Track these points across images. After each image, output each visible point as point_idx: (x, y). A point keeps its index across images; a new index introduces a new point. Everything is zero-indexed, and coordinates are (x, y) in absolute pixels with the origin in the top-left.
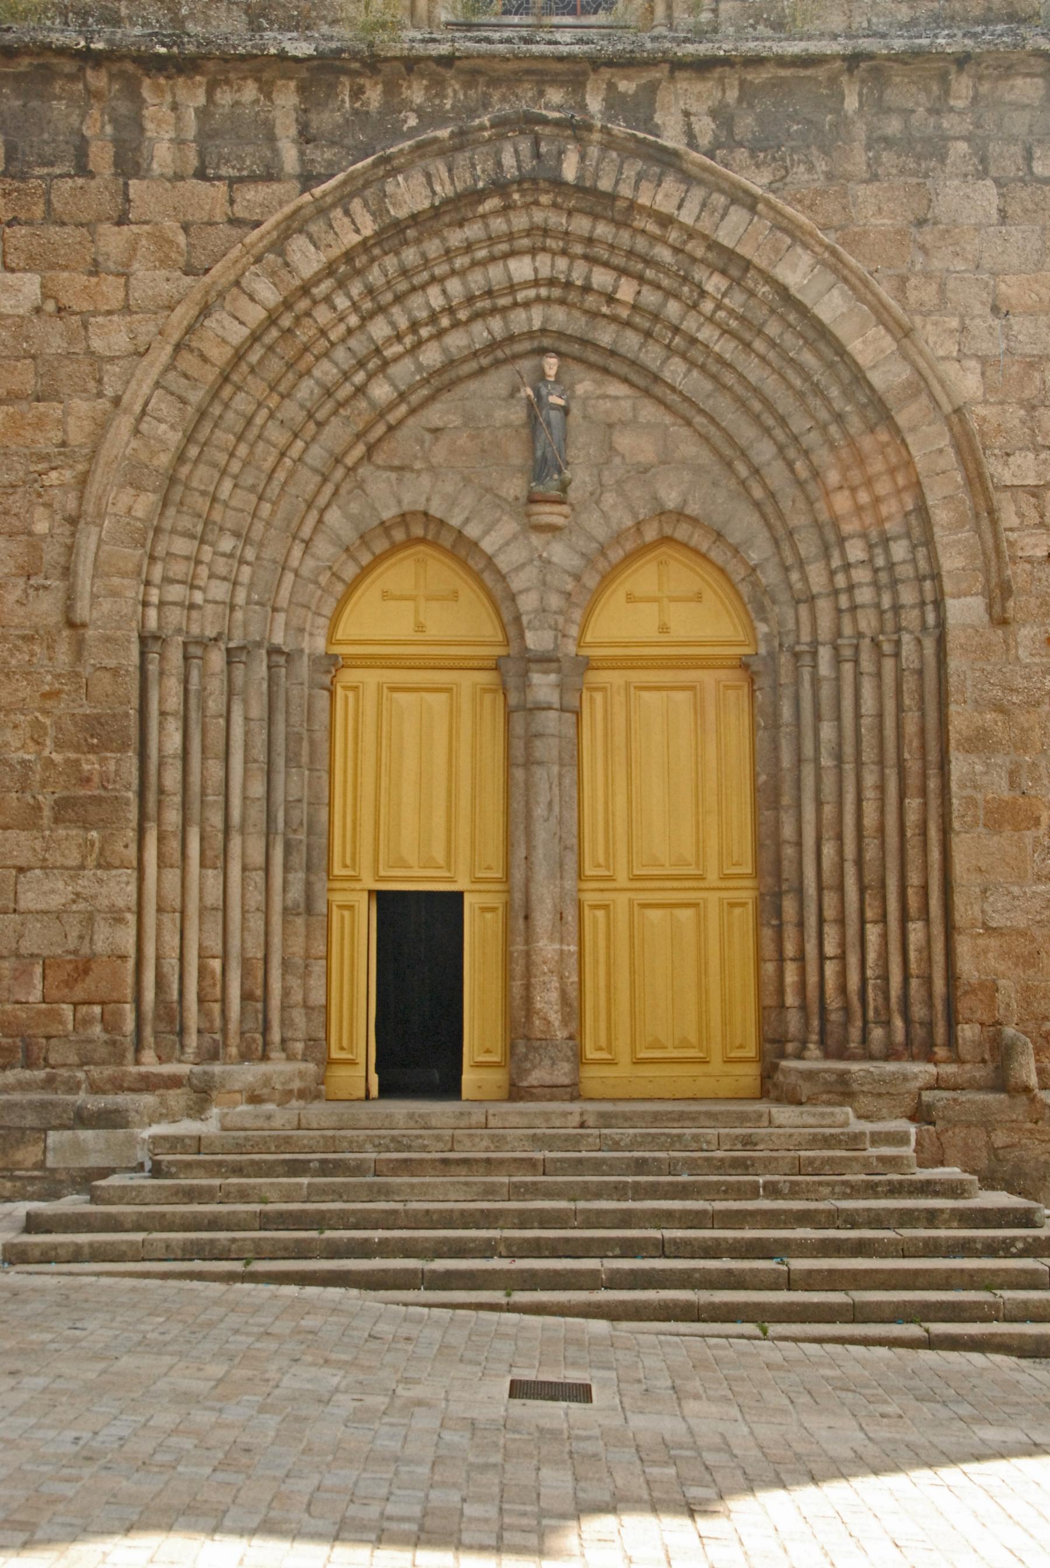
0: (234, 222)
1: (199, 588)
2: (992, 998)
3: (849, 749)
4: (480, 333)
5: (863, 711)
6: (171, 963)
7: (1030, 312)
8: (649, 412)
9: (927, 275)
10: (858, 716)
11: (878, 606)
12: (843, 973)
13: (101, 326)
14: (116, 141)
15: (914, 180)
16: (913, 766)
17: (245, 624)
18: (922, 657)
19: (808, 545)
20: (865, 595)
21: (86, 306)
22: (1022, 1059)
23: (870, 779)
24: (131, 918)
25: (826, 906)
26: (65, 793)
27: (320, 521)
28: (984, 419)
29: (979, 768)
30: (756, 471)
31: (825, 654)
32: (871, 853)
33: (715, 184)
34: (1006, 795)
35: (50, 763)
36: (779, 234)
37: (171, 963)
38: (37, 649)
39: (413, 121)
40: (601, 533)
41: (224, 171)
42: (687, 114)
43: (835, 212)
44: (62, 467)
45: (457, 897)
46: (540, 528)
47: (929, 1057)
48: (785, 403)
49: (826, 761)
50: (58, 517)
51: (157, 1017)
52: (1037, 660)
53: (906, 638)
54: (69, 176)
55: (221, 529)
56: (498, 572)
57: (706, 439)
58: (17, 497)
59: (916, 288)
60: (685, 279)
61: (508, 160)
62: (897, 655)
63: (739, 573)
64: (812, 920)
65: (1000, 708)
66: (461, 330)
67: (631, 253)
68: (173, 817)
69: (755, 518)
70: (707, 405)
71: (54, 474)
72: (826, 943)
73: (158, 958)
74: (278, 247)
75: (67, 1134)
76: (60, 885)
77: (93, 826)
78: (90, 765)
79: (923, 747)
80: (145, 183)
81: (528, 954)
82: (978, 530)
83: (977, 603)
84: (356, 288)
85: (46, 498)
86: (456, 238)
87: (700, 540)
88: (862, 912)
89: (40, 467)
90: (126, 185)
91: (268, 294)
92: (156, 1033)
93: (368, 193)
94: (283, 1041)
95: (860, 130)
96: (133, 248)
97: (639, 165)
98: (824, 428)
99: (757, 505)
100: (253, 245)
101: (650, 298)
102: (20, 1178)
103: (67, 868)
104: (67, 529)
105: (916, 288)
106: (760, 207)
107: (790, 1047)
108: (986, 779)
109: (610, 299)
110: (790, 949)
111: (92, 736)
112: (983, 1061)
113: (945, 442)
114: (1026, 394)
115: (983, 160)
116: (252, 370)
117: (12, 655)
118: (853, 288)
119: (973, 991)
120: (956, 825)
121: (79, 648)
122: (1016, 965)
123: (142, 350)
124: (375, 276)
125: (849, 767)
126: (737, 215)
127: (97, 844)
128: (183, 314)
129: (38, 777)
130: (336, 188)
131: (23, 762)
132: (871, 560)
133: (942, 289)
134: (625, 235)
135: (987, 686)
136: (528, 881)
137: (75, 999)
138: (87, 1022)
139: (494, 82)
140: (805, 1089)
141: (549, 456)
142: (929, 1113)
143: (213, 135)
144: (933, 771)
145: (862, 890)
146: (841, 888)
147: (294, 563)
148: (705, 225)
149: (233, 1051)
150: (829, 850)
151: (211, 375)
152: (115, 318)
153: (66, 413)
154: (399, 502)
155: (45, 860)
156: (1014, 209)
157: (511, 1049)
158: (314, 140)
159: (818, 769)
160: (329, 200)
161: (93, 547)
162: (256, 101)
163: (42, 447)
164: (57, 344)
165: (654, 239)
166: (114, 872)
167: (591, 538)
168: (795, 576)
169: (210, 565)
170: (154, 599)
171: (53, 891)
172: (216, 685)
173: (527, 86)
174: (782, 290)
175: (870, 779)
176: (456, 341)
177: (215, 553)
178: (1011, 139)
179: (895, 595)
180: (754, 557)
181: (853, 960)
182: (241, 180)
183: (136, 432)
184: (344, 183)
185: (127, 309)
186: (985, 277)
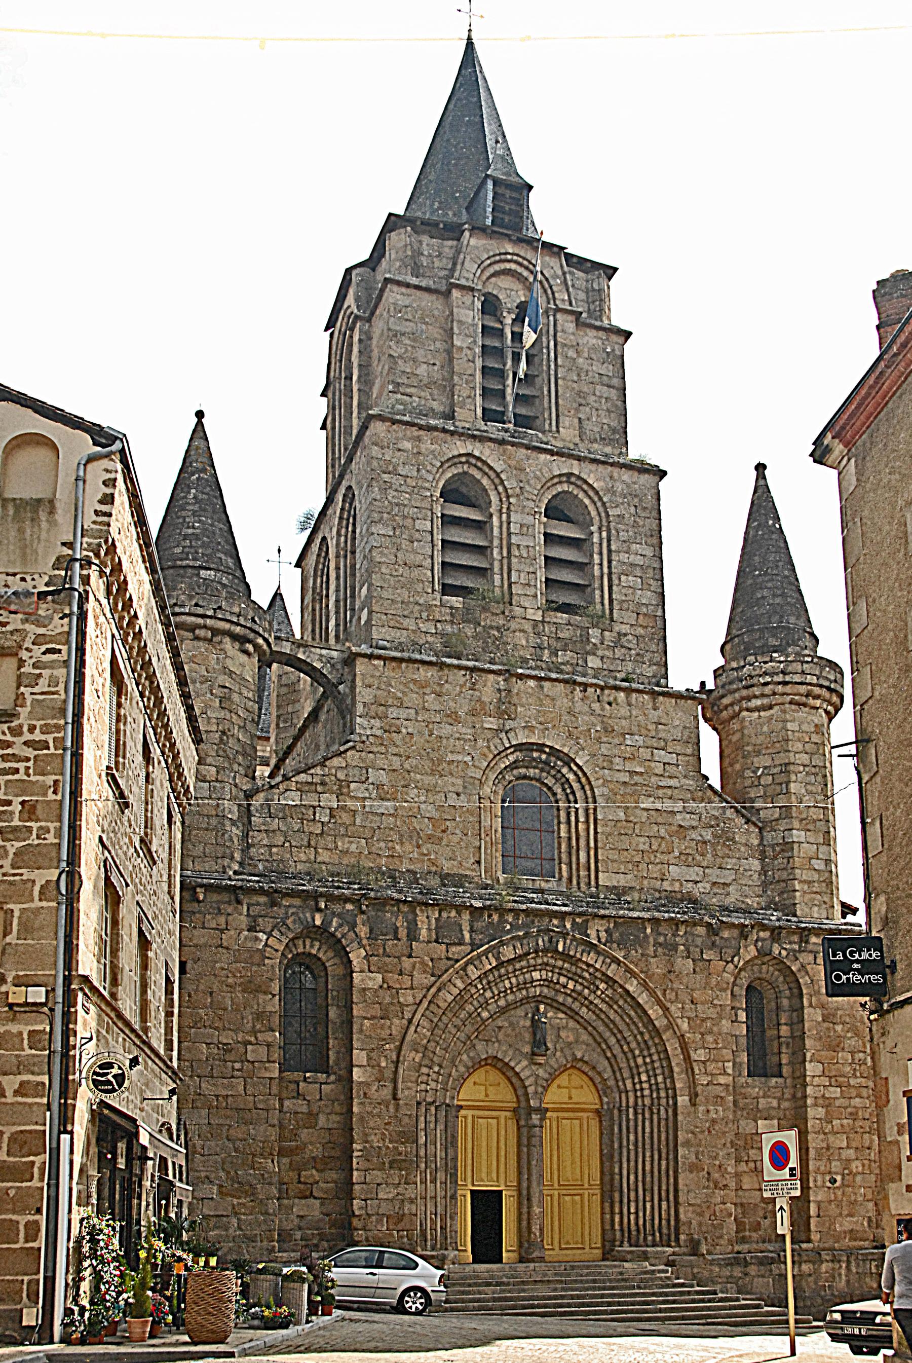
3: (640, 1144)
7: (702, 1003)
8: (572, 1024)
14: (408, 928)
20: (647, 1092)
21: (398, 986)
30: (609, 1047)
31: (631, 1110)
33: (606, 955)
34: (695, 1161)
35: (388, 1148)
39: (508, 927)
46: (536, 1064)
47: (669, 1246)
48: (622, 1026)
49: (631, 1147)
57: (591, 1034)
60: (593, 984)
61: (540, 943)
63: (597, 1080)
64: (625, 1200)
65: (693, 1133)
67: (575, 974)
68: (423, 1166)
69: (606, 1063)
70: (594, 1024)
74: (464, 969)
78: (402, 1148)
79: (667, 1144)
81: (529, 1213)
82: (687, 1073)
83: (687, 1098)
86: (518, 966)
87: (586, 1068)
95: (651, 940)
96: (414, 967)
99: (608, 1058)
101: (579, 988)
107: (617, 1243)
109: (565, 987)
110: (617, 1210)
113: (677, 1045)
121: (397, 1109)
125: (640, 1150)
126: (614, 966)
134: (574, 968)
136: (529, 1188)
138: (402, 1237)
139: (536, 916)
143: (441, 927)
145: (644, 1190)
148: (604, 969)
150: (632, 1177)
151: (441, 1012)
156: (697, 969)
157: (520, 1245)
163: (383, 1036)
164: (388, 1000)
165: (583, 970)
168: (620, 1083)
174: (627, 992)
176: (510, 998)
178: (697, 946)
179: (658, 1093)
181: (641, 1214)
183: (416, 1031)
185: (412, 988)
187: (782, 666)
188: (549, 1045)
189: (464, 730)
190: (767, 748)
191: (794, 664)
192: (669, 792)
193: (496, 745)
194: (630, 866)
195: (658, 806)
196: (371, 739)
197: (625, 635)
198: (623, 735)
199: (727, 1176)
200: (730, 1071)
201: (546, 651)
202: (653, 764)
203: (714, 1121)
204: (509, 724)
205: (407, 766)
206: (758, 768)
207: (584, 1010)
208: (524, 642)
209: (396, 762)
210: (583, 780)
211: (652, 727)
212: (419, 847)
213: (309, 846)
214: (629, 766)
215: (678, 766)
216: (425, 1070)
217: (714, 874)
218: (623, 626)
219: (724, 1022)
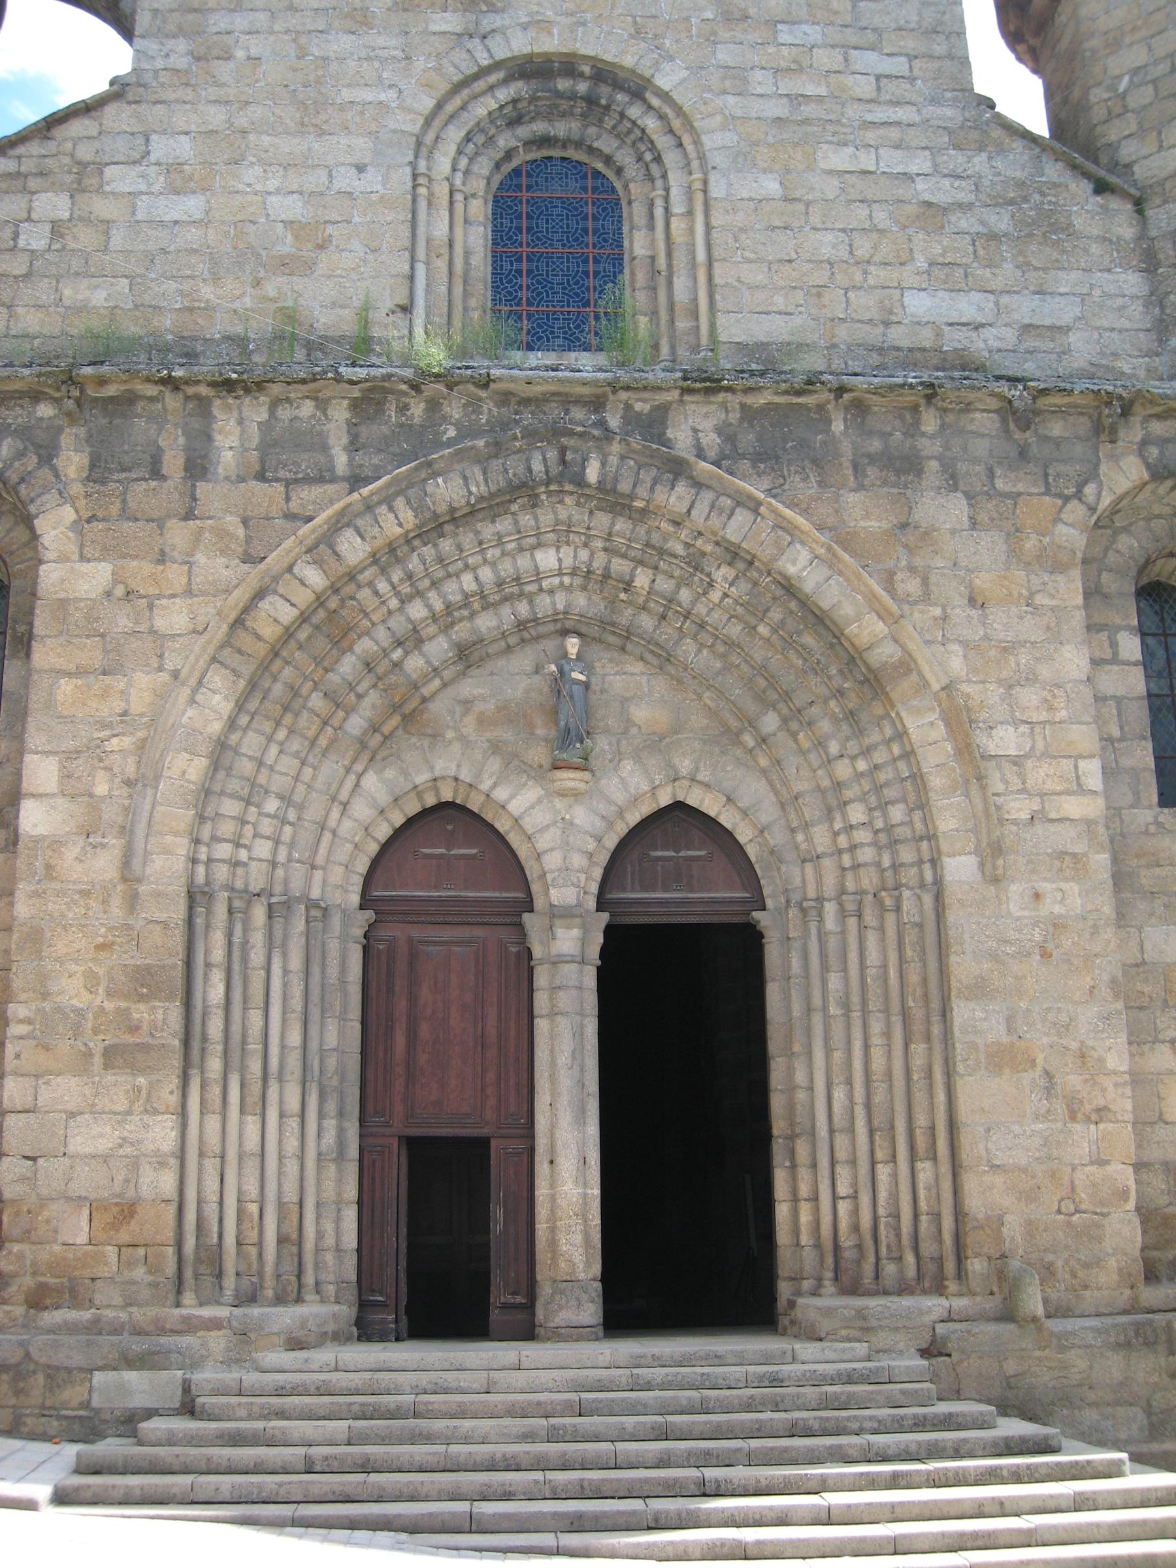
0: (290, 516)
1: (245, 846)
3: (855, 999)
4: (507, 616)
5: (868, 963)
6: (211, 1210)
10: (863, 967)
11: (878, 864)
12: (856, 1211)
13: (164, 608)
14: (188, 449)
15: (896, 491)
16: (918, 1013)
17: (286, 882)
18: (921, 911)
19: (811, 809)
20: (866, 855)
21: (153, 591)
22: (1030, 1290)
23: (876, 1027)
24: (174, 1162)
25: (837, 1147)
26: (115, 1041)
27: (357, 785)
28: (968, 695)
29: (979, 1014)
31: (830, 908)
32: (879, 1098)
34: (1005, 1039)
36: (780, 533)
37: (211, 1210)
38: (93, 903)
39: (452, 433)
40: (620, 797)
41: (281, 474)
42: (695, 431)
43: (828, 515)
44: (123, 734)
45: (483, 1143)
46: (562, 794)
47: (939, 1289)
49: (834, 1010)
50: (117, 780)
51: (198, 1259)
52: (1026, 913)
53: (906, 893)
55: (266, 792)
56: (524, 832)
58: (80, 761)
59: (902, 581)
62: (898, 909)
65: (994, 957)
66: (491, 611)
68: (215, 1065)
71: (115, 741)
72: (838, 1183)
73: (199, 1202)
75: (111, 1375)
76: (108, 1129)
77: (141, 1071)
80: (210, 485)
84: (397, 575)
85: (107, 763)
88: (872, 1152)
89: (102, 735)
90: (194, 486)
91: (315, 578)
92: (197, 1276)
93: (411, 492)
94: (317, 1284)
97: (654, 472)
100: (305, 537)
102: (66, 1418)
103: (116, 1113)
104: (125, 791)
105: (902, 581)
106: (762, 509)
108: (985, 1024)
111: (142, 986)
112: (992, 1293)
114: (1004, 674)
115: (953, 476)
116: (300, 647)
118: (847, 580)
119: (981, 1228)
120: (960, 1068)
122: (1019, 1200)
123: (201, 629)
124: (414, 563)
127: (144, 1092)
128: (240, 596)
129: (90, 1025)
130: (380, 489)
132: (871, 823)
133: (925, 582)
135: (982, 938)
137: (120, 1242)
140: (825, 1326)
141: (572, 726)
142: (944, 1344)
144: (936, 1019)
145: (871, 1132)
146: (851, 1130)
147: (332, 822)
149: (270, 1293)
151: (261, 649)
152: (177, 600)
153: (130, 684)
155: (94, 1105)
156: (983, 517)
158: (364, 446)
159: (827, 1018)
160: (375, 498)
161: (148, 807)
162: (314, 416)
164: (124, 623)
166: (160, 1118)
167: (610, 802)
169: (255, 825)
170: (203, 857)
171: (101, 1136)
173: (554, 405)
175: (876, 1027)
177: (260, 814)
178: (975, 460)
180: (764, 818)
181: (865, 1199)
182: (296, 481)
183: (192, 701)
184: (389, 485)
185: (189, 592)
189: (381, 41)
190: (1134, 29)
192: (894, 134)
193: (460, 64)
194: (799, 297)
195: (867, 161)
196: (164, 77)
199: (1108, 1082)
202: (849, 80)
203: (1058, 925)
204: (495, 21)
205: (242, 121)
206: (1119, 77)
207: (688, 645)
209: (216, 117)
210: (676, 124)
212: (257, 283)
214: (789, 85)
215: (912, 80)
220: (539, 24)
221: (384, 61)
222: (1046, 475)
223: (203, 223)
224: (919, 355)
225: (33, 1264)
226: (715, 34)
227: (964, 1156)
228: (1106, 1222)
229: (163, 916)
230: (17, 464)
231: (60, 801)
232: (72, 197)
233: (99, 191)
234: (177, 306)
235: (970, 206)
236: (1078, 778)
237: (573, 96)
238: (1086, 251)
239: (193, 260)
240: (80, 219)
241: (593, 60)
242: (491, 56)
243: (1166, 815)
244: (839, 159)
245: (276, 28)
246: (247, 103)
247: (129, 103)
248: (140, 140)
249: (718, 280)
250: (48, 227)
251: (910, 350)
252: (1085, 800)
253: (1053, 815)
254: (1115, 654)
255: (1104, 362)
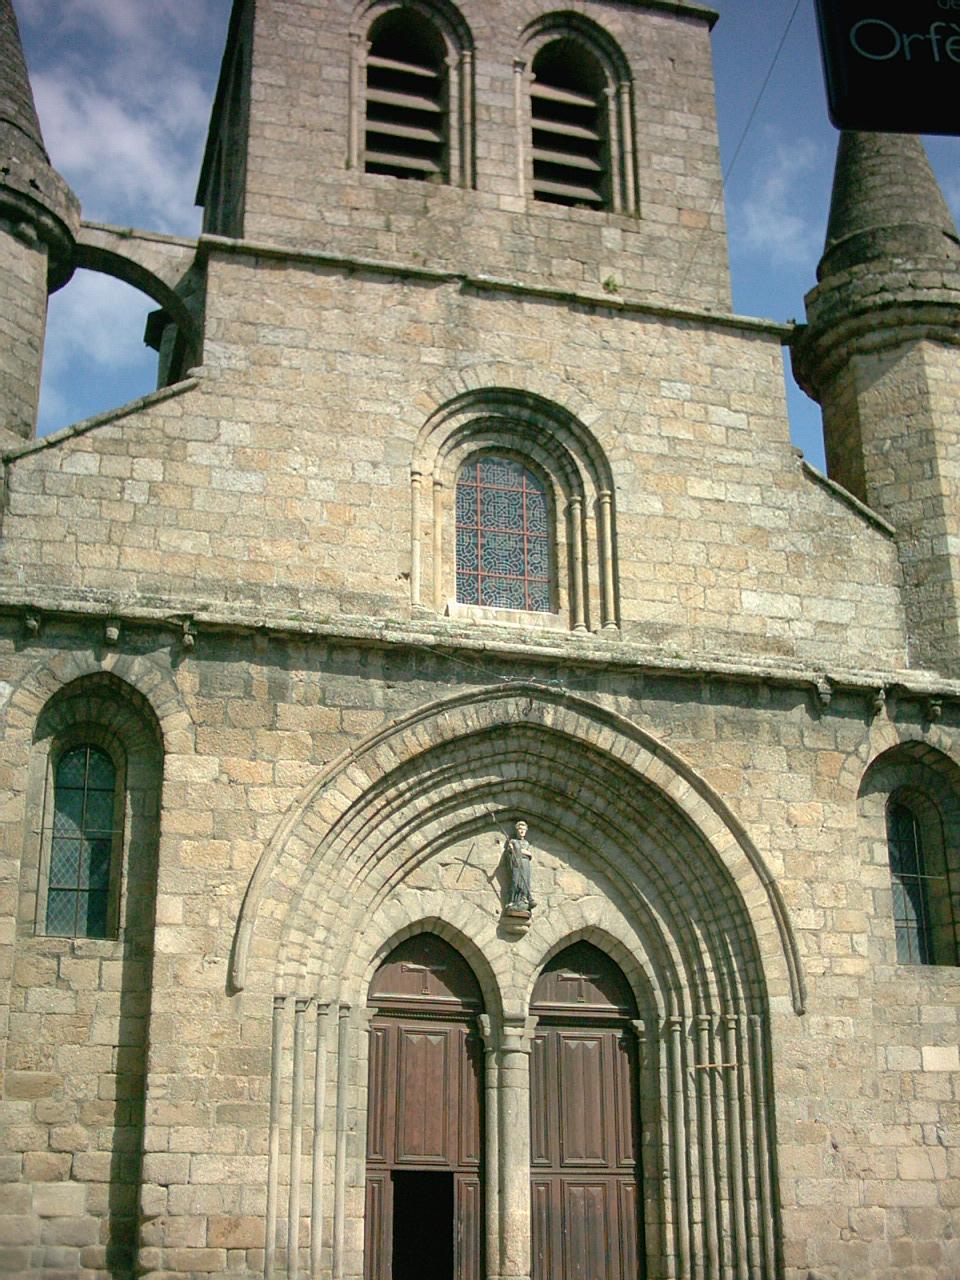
2: (804, 1251)
9: (751, 799)
29: (792, 1104)
34: (807, 1121)
45: (448, 1177)
54: (239, 698)
68: (287, 1119)
71: (223, 887)
76: (221, 1166)
78: (242, 1082)
80: (287, 706)
89: (214, 882)
98: (689, 886)
103: (225, 1154)
117: (192, 1007)
127: (246, 1138)
131: (197, 1080)
138: (237, 1261)
150: (695, 1151)
152: (266, 788)
154: (423, 910)
165: (593, 763)
171: (215, 1170)
172: (311, 1029)
182: (347, 708)
186: (783, 802)
187: (910, 276)
188: (535, 897)
191: (931, 274)
197: (661, 239)
198: (656, 382)
199: (870, 1151)
200: (862, 949)
201: (532, 257)
203: (839, 1045)
205: (288, 418)
208: (495, 244)
209: (269, 412)
211: (703, 370)
213: (109, 541)
216: (295, 936)
217: (818, 609)
218: (659, 226)
219: (848, 860)
220: (495, 363)
221: (389, 381)
222: (836, 737)
223: (262, 495)
224: (750, 639)
225: (165, 1262)
226: (618, 384)
227: (782, 1198)
228: (869, 1246)
229: (259, 1015)
230: (146, 678)
231: (184, 929)
232: (163, 464)
233: (183, 460)
234: (246, 559)
235: (785, 531)
236: (853, 946)
237: (518, 420)
238: (859, 568)
239: (256, 523)
240: (170, 482)
241: (537, 398)
242: (466, 386)
243: (918, 985)
244: (700, 488)
245: (310, 346)
246: (291, 404)
247: (203, 393)
248: (214, 424)
249: (621, 574)
250: (147, 486)
251: (745, 635)
252: (858, 961)
253: (837, 971)
254: (872, 858)
255: (868, 651)
